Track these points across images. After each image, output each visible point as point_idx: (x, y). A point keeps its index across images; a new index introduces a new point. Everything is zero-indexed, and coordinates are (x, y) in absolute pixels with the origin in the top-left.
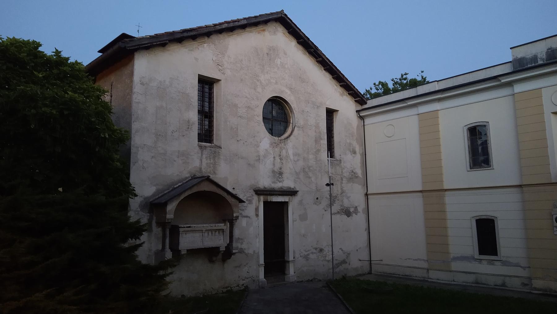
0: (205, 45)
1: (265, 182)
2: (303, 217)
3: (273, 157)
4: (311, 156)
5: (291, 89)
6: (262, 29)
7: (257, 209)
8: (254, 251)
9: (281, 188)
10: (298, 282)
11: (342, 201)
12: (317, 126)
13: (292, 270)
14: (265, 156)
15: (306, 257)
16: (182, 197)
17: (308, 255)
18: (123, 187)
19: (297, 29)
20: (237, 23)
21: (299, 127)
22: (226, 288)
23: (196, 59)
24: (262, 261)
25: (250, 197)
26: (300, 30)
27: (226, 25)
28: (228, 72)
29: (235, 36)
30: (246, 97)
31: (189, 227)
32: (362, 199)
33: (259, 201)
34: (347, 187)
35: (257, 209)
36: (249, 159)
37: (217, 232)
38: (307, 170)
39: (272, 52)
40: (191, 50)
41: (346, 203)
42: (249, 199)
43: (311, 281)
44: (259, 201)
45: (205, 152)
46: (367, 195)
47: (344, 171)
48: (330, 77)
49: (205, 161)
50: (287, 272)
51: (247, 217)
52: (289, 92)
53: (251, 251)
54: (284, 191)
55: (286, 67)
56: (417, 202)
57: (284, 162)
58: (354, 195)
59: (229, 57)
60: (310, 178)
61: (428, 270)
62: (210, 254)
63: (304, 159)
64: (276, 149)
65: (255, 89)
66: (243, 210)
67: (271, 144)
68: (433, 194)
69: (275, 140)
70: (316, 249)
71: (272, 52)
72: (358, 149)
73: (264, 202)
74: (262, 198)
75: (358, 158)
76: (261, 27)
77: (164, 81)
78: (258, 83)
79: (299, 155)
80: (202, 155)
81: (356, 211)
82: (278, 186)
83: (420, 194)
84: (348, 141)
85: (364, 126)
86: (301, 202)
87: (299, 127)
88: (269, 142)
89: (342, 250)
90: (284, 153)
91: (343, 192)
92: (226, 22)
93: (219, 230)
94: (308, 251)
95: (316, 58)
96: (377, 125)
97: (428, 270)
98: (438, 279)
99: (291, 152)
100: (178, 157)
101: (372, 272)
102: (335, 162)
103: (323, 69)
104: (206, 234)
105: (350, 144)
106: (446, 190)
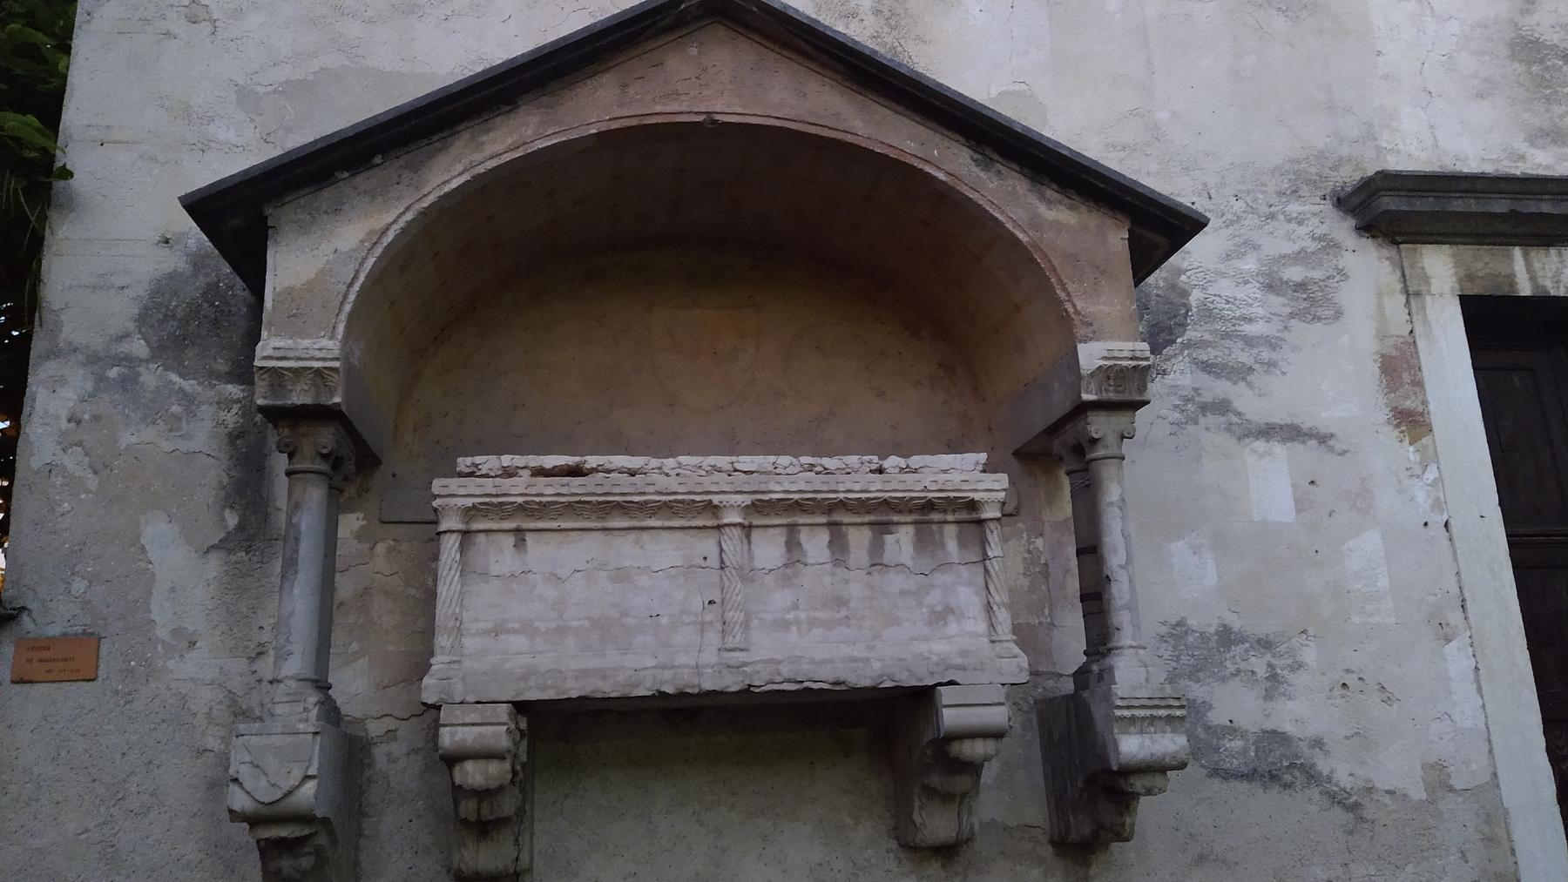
7: (1399, 367)
8: (1438, 779)
16: (452, 169)
25: (1300, 257)
31: (576, 471)
33: (1412, 293)
35: (1399, 367)
37: (901, 543)
42: (1294, 274)
44: (1412, 293)
51: (1293, 433)
53: (1396, 770)
62: (877, 733)
66: (1240, 373)
73: (1467, 302)
74: (1441, 268)
104: (768, 549)
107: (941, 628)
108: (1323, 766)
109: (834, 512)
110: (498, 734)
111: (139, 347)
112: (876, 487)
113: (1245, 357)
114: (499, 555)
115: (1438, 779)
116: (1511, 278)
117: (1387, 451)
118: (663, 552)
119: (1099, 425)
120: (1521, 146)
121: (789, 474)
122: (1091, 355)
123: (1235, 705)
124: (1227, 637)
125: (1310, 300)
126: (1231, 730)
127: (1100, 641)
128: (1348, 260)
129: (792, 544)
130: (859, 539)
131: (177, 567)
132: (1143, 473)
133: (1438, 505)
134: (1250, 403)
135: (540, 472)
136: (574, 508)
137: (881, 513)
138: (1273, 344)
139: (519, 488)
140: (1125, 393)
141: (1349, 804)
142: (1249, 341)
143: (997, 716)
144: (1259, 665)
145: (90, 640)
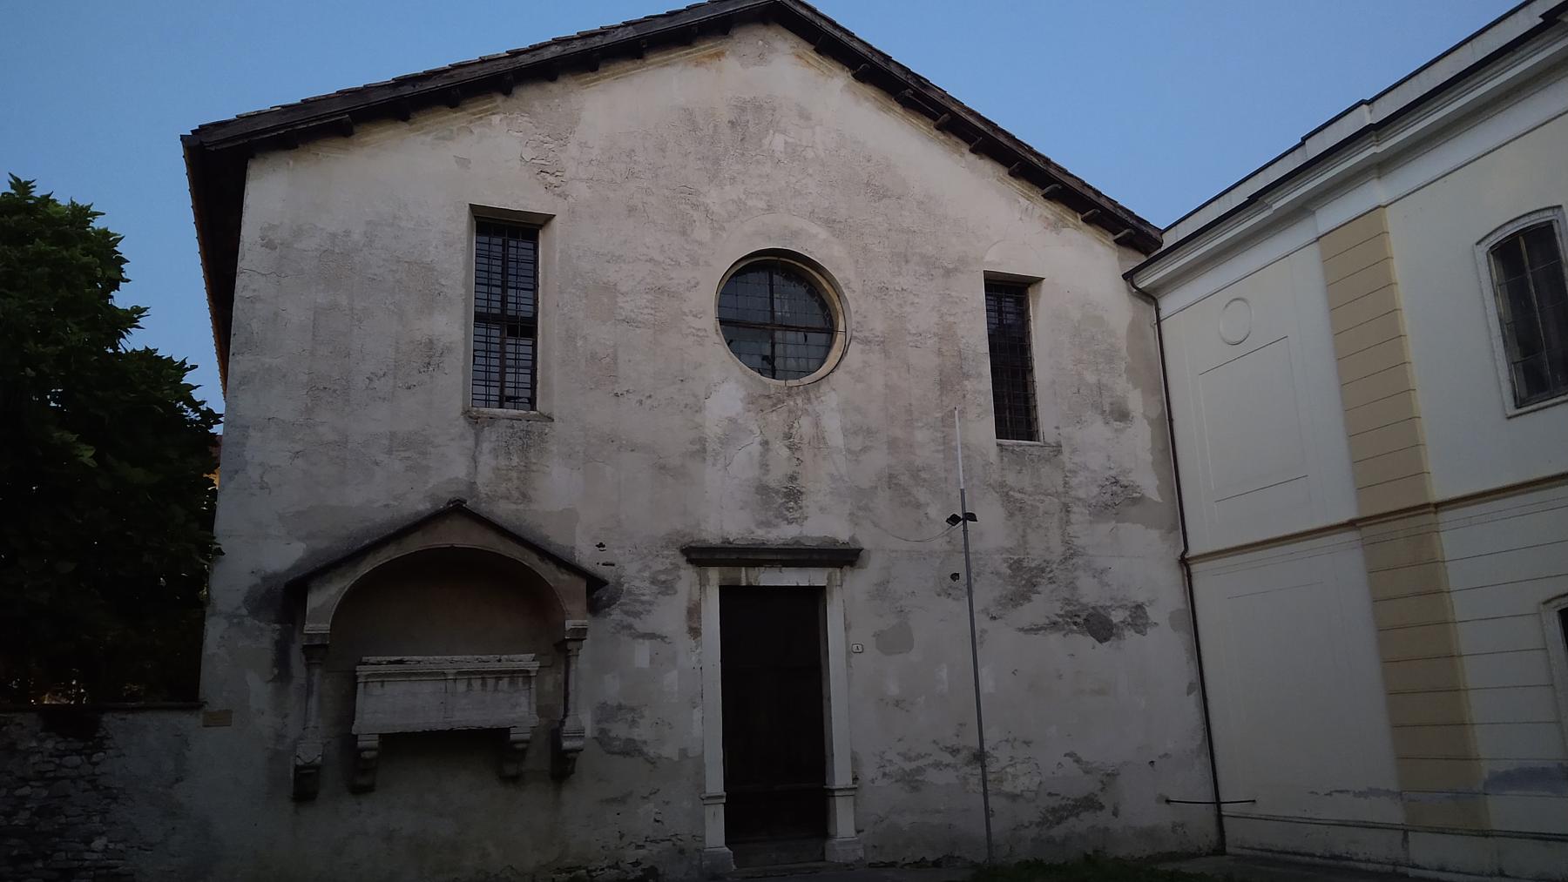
0: (496, 119)
1: (728, 522)
2: (894, 641)
3: (758, 439)
4: (921, 436)
5: (829, 223)
6: (713, 51)
8: (684, 753)
9: (797, 542)
10: (871, 865)
11: (1071, 584)
12: (947, 334)
13: (844, 821)
14: (725, 441)
15: (912, 781)
16: (365, 568)
17: (919, 770)
18: (201, 542)
19: (838, 34)
20: (597, 39)
21: (866, 341)
22: (569, 870)
23: (463, 162)
24: (715, 782)
25: (665, 571)
26: (851, 35)
27: (557, 50)
28: (581, 191)
29: (603, 84)
30: (651, 260)
31: (401, 662)
32: (1170, 578)
34: (1092, 535)
35: (694, 612)
36: (656, 447)
37: (506, 681)
38: (905, 479)
39: (750, 120)
40: (444, 138)
41: (1090, 593)
42: (662, 577)
43: (937, 864)
44: (703, 584)
45: (491, 437)
46: (1184, 562)
47: (1074, 482)
48: (1002, 171)
49: (487, 461)
50: (831, 831)
51: (652, 636)
52: (823, 234)
53: (670, 751)
54: (811, 551)
55: (810, 154)
56: (1344, 564)
57: (807, 455)
58: (1134, 563)
59: (583, 145)
60: (918, 506)
61: (1406, 832)
62: (488, 747)
63: (893, 444)
64: (774, 416)
65: (684, 233)
66: (637, 615)
67: (751, 400)
68: (1396, 523)
69: (766, 386)
70: (954, 751)
71: (750, 120)
72: (1136, 402)
73: (721, 588)
74: (714, 575)
75: (1139, 438)
76: (706, 48)
77: (347, 233)
78: (696, 215)
79: (869, 432)
80: (477, 444)
81: (1138, 618)
82: (783, 533)
83: (1351, 536)
84: (1091, 378)
85: (1159, 321)
86: (881, 590)
87: (866, 341)
88: (742, 393)
89: (1078, 761)
90: (805, 426)
91: (1071, 553)
92: (557, 42)
93: (513, 674)
94: (919, 757)
95: (933, 117)
96: (1200, 312)
97: (1406, 832)
98: (1442, 869)
99: (833, 425)
100: (390, 452)
101: (1228, 849)
102: (1036, 452)
103: (965, 149)
104: (462, 686)
105: (1100, 387)
106: (1439, 506)
107: (515, 711)
108: (645, 749)
109: (483, 675)
110: (375, 743)
111: (244, 611)
112: (497, 667)
113: (639, 608)
114: (376, 689)
115: (684, 753)
116: (739, 580)
117: (684, 642)
118: (427, 688)
119: (570, 645)
120: (753, 528)
121: (469, 661)
122: (569, 624)
123: (619, 730)
124: (620, 707)
125: (666, 587)
126: (617, 738)
127: (565, 716)
128: (682, 573)
129: (469, 684)
130: (491, 682)
131: (258, 687)
132: (583, 661)
133: (699, 661)
134: (640, 626)
135: (390, 662)
136: (400, 675)
137: (498, 675)
138: (651, 603)
139: (383, 669)
140: (580, 635)
141: (652, 762)
142: (643, 603)
143: (527, 736)
144: (629, 717)
145: (229, 712)
